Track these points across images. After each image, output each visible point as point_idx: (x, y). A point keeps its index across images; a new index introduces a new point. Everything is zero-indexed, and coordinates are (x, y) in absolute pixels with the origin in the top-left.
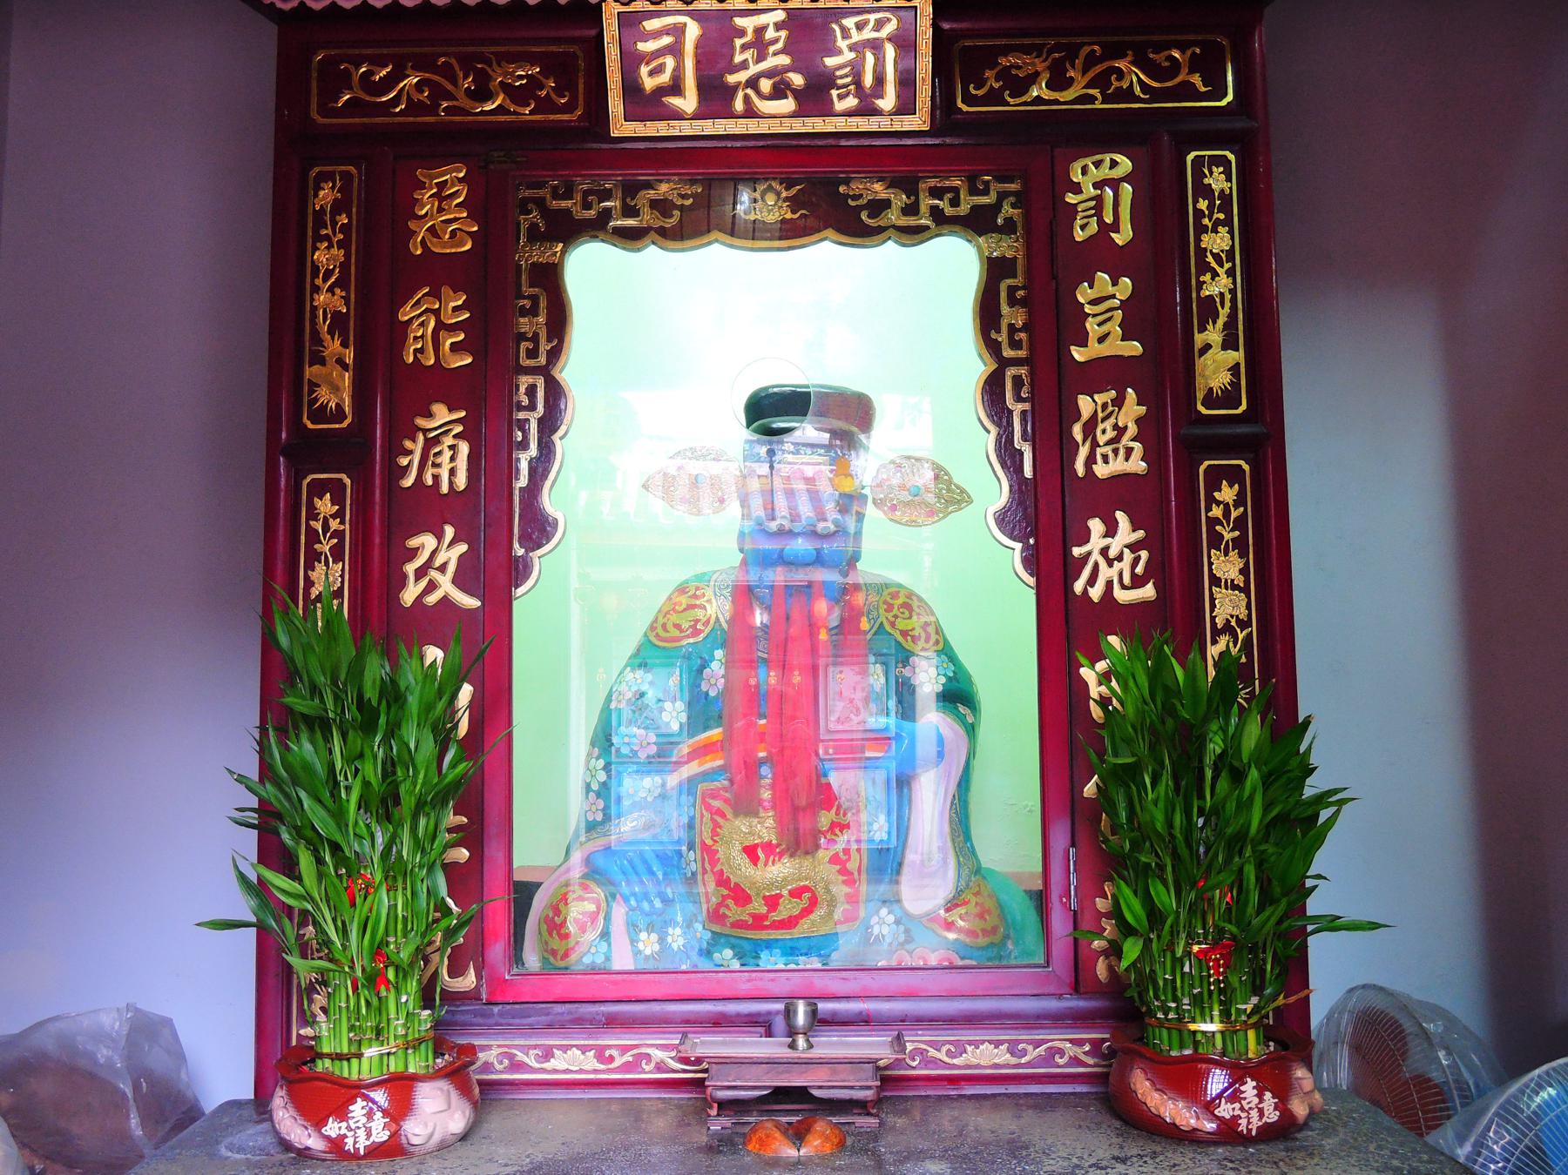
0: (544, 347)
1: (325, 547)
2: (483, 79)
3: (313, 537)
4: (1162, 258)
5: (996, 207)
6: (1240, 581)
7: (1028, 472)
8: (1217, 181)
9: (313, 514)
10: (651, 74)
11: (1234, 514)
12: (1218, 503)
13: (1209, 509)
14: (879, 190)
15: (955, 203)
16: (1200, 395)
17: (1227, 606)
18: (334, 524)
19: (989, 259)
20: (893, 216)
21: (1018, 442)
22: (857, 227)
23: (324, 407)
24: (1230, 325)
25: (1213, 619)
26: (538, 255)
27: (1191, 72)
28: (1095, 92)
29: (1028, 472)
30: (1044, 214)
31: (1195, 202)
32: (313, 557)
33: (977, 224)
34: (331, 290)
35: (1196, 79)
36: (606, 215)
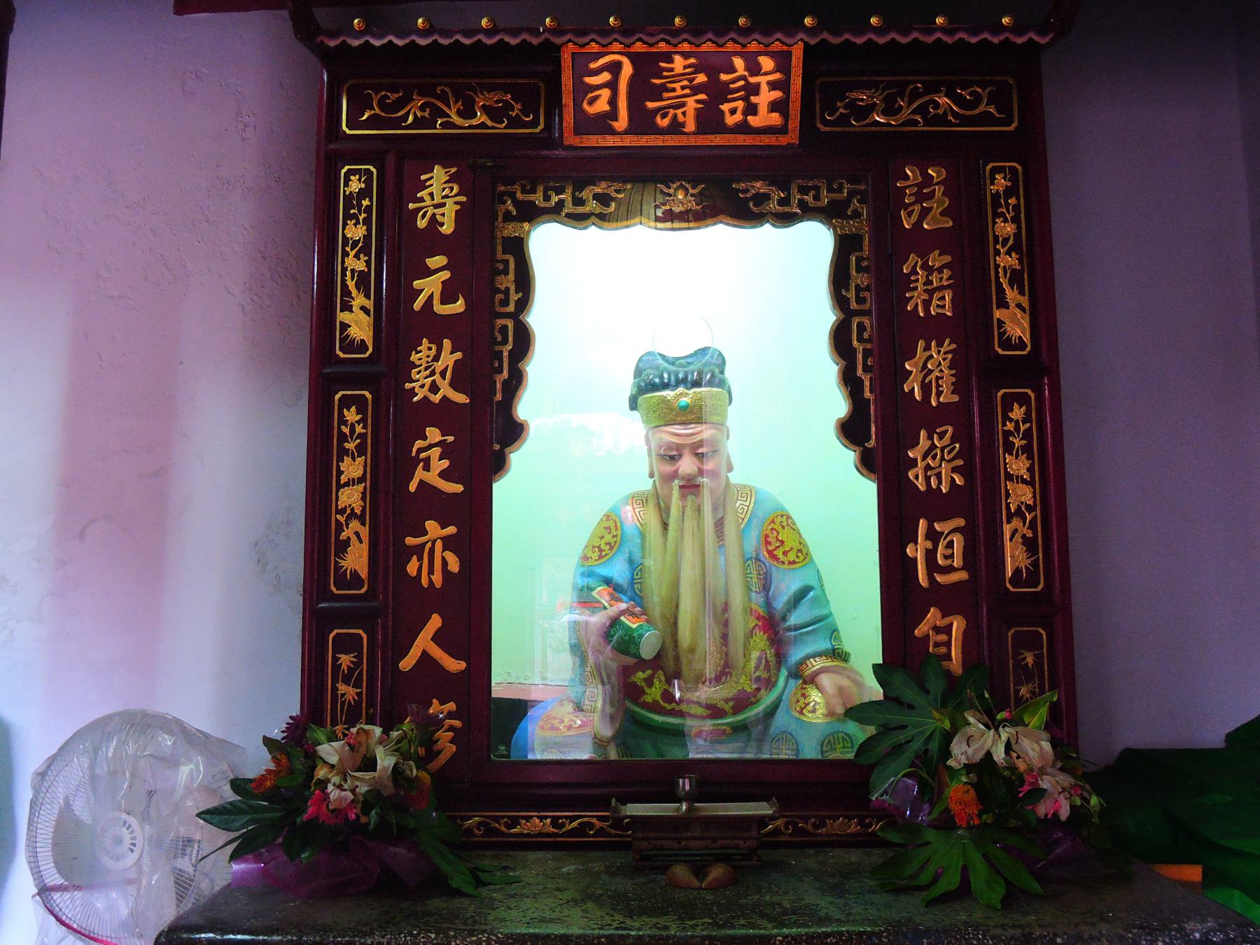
0: (514, 297)
12: (1011, 420)
13: (1004, 424)
14: (759, 186)
15: (817, 198)
18: (359, 429)
20: (773, 206)
22: (745, 213)
25: (1008, 505)
26: (510, 230)
30: (886, 205)
32: (343, 452)
33: (828, 214)
36: (561, 204)
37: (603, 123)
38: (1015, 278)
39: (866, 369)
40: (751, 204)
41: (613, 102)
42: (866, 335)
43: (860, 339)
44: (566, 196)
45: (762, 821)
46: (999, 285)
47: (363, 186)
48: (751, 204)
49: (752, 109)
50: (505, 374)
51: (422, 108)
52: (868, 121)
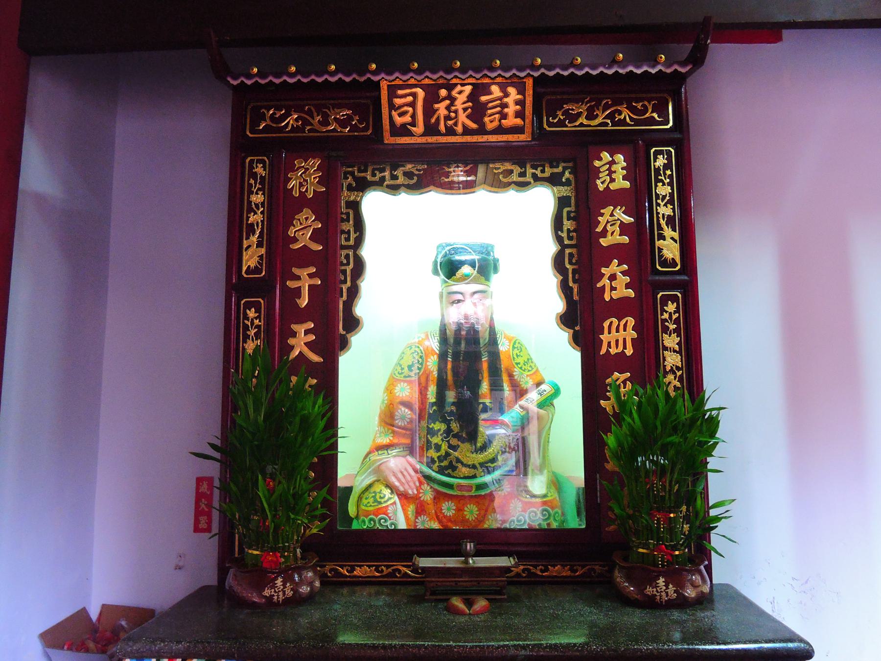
0: (353, 236)
1: (252, 332)
2: (326, 116)
3: (246, 328)
4: (638, 198)
5: (563, 173)
6: (677, 347)
7: (576, 297)
8: (259, 170)
9: (246, 317)
10: (400, 115)
11: (674, 317)
12: (666, 312)
13: (662, 315)
14: (508, 166)
15: (543, 171)
16: (244, 268)
17: (672, 360)
19: (559, 198)
20: (515, 177)
21: (571, 284)
23: (666, 260)
24: (261, 235)
25: (665, 366)
27: (652, 112)
28: (609, 121)
29: (576, 297)
30: (585, 177)
31: (249, 180)
32: (246, 337)
33: (554, 181)
34: (665, 205)
35: (655, 115)
36: (383, 179)
37: (403, 130)
38: (670, 221)
39: (574, 281)
40: (501, 177)
41: (413, 116)
42: (574, 261)
43: (570, 263)
44: (387, 174)
45: (507, 570)
46: (659, 225)
47: (666, 162)
48: (501, 177)
49: (504, 116)
50: (349, 284)
51: (296, 120)
52: (577, 123)
